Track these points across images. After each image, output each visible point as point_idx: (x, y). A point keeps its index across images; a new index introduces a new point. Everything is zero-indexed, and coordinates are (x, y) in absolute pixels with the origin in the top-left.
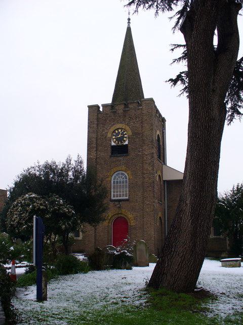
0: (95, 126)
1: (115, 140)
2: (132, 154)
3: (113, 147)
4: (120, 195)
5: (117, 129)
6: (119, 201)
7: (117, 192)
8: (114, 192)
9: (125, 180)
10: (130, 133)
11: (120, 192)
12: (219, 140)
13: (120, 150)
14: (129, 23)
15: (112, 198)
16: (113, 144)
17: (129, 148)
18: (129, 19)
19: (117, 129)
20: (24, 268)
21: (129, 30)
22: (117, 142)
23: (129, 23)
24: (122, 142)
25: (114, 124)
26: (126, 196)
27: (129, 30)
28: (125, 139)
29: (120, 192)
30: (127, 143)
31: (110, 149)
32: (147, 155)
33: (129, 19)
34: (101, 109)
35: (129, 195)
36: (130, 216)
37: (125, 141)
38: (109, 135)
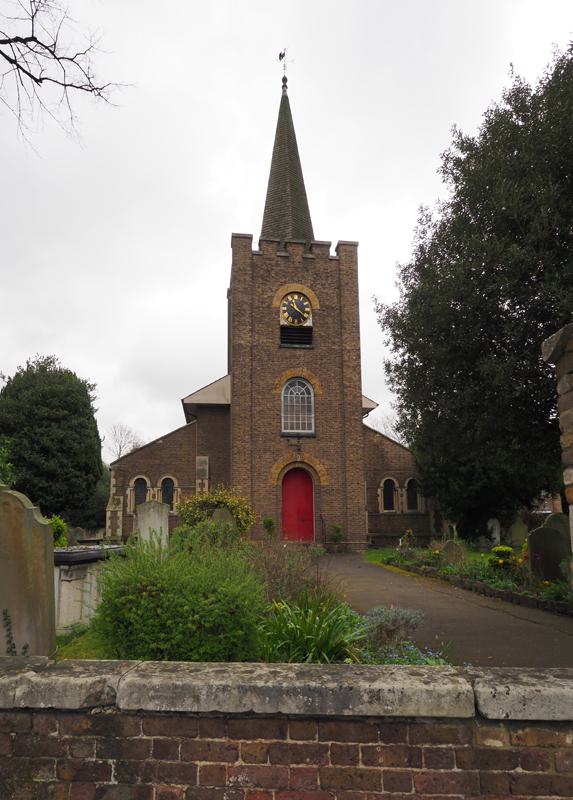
0: (248, 278)
1: (286, 314)
2: (321, 346)
3: (283, 329)
4: (298, 424)
5: (292, 293)
6: (299, 436)
7: (292, 419)
8: (286, 418)
9: (306, 396)
10: (316, 305)
11: (298, 419)
12: (245, 340)
13: (296, 335)
14: (285, 86)
15: (283, 431)
16: (283, 322)
17: (315, 335)
18: (285, 80)
19: (292, 293)
20: (148, 539)
21: (285, 101)
22: (290, 319)
23: (285, 86)
24: (299, 322)
25: (285, 282)
26: (310, 428)
27: (285, 101)
28: (306, 315)
29: (292, 419)
30: (309, 323)
31: (278, 332)
32: (349, 352)
33: (285, 80)
34: (333, 253)
35: (316, 427)
36: (319, 467)
37: (305, 319)
38: (276, 303)
